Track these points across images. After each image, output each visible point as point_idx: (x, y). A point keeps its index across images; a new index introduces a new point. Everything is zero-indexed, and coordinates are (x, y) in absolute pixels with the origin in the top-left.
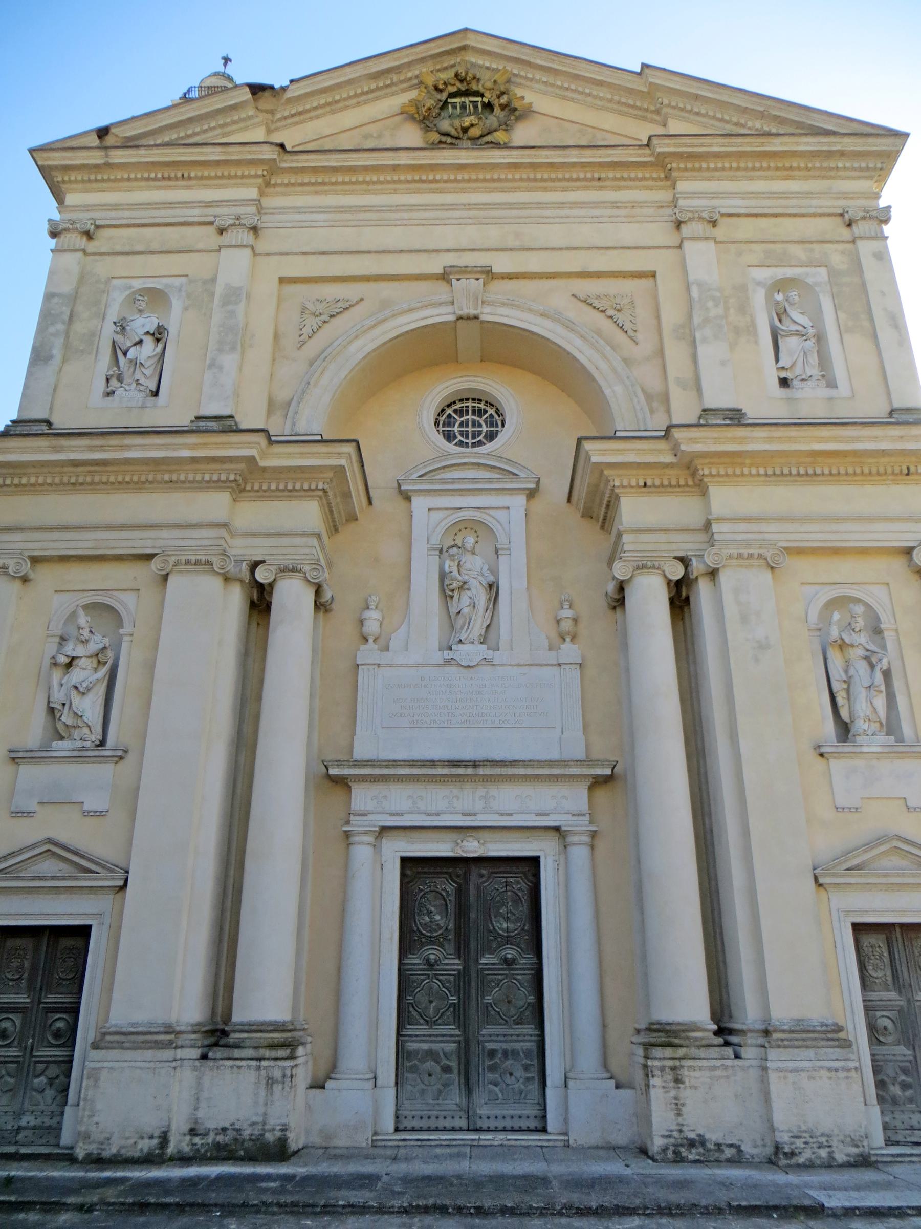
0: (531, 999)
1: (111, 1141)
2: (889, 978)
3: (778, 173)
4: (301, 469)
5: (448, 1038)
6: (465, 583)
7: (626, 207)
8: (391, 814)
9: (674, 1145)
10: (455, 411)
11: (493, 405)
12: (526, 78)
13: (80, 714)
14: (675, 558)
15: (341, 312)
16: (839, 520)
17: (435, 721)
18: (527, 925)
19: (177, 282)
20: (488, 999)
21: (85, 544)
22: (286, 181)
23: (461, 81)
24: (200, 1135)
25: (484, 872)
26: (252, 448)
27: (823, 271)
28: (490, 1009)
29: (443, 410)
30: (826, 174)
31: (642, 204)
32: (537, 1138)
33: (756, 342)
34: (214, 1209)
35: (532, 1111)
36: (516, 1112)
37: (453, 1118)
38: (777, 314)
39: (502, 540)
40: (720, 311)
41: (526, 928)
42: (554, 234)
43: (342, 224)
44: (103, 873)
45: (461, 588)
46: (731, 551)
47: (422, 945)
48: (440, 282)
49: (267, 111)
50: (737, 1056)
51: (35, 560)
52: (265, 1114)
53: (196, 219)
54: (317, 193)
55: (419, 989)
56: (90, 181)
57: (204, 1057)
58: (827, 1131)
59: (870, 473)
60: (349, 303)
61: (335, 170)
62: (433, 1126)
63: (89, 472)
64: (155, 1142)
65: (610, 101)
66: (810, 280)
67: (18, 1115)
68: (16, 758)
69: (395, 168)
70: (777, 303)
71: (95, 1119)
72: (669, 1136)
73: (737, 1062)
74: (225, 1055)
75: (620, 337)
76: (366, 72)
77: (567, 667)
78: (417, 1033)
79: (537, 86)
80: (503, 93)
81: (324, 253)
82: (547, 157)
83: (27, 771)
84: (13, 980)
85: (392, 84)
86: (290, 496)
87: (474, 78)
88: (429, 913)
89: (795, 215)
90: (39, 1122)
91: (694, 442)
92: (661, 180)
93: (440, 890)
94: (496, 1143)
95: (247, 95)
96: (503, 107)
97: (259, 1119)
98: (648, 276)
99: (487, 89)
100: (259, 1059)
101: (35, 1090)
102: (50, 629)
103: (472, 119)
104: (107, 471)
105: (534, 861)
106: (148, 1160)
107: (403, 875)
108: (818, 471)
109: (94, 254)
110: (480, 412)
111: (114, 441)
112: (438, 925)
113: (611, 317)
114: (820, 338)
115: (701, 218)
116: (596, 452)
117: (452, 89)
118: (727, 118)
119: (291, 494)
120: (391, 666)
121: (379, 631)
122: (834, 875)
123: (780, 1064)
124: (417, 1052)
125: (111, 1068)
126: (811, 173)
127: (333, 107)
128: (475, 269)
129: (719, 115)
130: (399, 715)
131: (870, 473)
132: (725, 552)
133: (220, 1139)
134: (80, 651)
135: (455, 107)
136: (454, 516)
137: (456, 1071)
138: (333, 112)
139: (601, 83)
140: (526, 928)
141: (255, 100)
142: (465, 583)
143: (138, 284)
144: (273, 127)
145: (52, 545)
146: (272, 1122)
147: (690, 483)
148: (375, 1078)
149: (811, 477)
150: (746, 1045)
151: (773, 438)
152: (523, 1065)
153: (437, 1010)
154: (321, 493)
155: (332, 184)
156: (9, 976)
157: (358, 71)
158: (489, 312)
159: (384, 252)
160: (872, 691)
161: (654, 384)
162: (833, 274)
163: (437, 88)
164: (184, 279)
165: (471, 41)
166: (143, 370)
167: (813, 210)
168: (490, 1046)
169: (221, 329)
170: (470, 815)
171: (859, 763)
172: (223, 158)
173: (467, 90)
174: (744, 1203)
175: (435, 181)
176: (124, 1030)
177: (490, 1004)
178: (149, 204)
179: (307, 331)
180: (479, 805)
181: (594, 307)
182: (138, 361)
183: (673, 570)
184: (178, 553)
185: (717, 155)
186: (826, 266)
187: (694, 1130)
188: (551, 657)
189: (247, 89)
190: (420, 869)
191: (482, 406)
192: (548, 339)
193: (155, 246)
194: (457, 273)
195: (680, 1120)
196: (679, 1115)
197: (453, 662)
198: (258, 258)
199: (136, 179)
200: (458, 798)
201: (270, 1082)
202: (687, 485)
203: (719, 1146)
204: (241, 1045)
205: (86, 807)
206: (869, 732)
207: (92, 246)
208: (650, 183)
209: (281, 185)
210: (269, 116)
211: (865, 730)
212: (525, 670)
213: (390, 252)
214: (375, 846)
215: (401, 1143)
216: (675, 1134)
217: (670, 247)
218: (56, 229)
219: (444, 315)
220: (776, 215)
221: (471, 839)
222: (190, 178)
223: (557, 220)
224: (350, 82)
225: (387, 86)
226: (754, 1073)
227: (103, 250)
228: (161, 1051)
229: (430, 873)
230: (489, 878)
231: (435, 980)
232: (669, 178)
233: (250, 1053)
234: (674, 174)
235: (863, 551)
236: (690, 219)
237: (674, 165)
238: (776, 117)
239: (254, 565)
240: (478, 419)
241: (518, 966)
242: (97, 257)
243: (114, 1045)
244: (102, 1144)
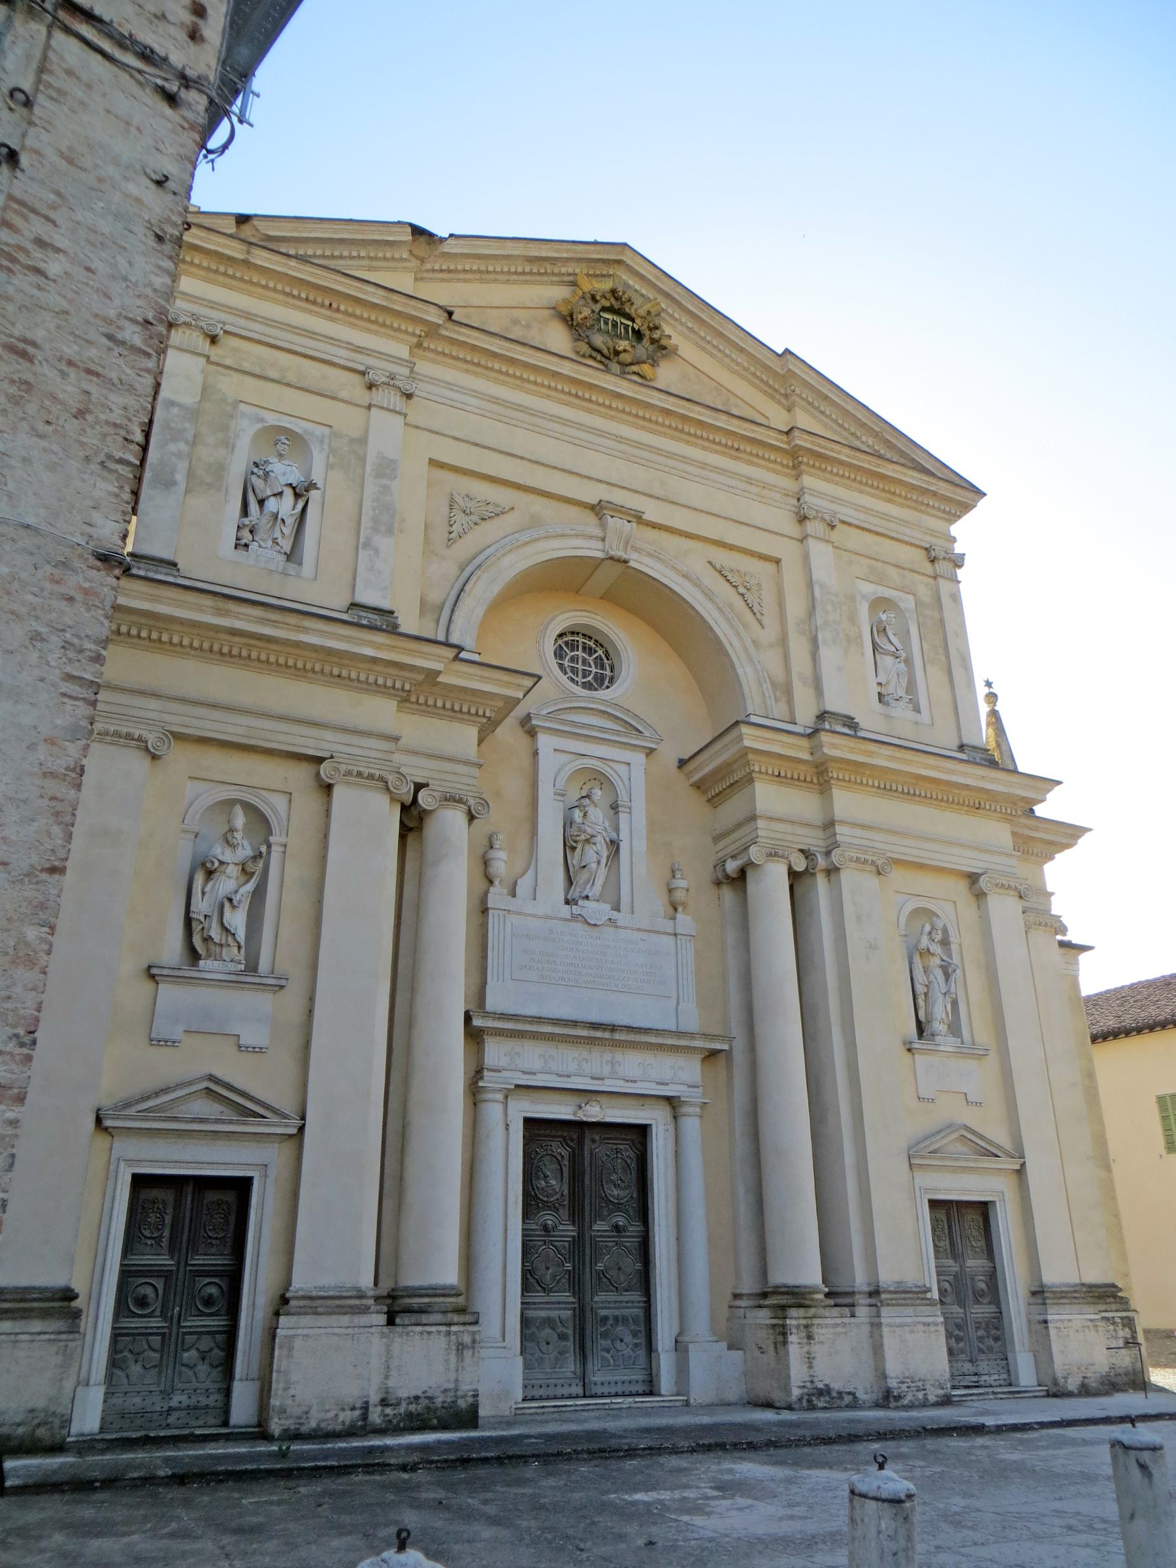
0: (639, 1266)
1: (309, 1415)
2: (948, 1247)
3: (884, 495)
4: (474, 692)
6: (593, 836)
7: (757, 486)
8: (525, 1073)
9: (808, 1395)
10: (566, 643)
12: (672, 316)
13: (233, 932)
14: (802, 851)
16: (928, 839)
19: (319, 430)
20: (600, 1266)
21: (234, 728)
22: (440, 349)
23: (617, 299)
24: (391, 1405)
27: (911, 597)
28: (601, 1275)
30: (918, 506)
34: (531, 1460)
35: (639, 1376)
36: (626, 1377)
37: (570, 1385)
42: (693, 493)
44: (275, 1119)
45: (587, 841)
46: (852, 854)
48: (588, 513)
50: (853, 1316)
52: (457, 1380)
53: (342, 362)
54: (467, 371)
56: (217, 271)
61: (494, 355)
62: (552, 1395)
64: (357, 1413)
65: (746, 369)
66: (901, 605)
67: (166, 1394)
69: (555, 374)
70: (881, 622)
71: (292, 1392)
72: (804, 1387)
73: (852, 1320)
74: (413, 1321)
76: (525, 253)
77: (683, 938)
79: (680, 328)
81: (477, 445)
82: (699, 413)
86: (452, 717)
88: (546, 1177)
89: (892, 538)
90: (193, 1401)
92: (787, 467)
93: (555, 1154)
94: (625, 1406)
97: (451, 1386)
98: (771, 561)
100: (449, 1325)
101: (187, 1366)
102: (186, 822)
105: (643, 1130)
106: (350, 1432)
109: (218, 364)
110: (591, 651)
111: (292, 619)
112: (554, 1190)
113: (742, 595)
114: (908, 662)
115: (823, 519)
118: (846, 425)
119: (455, 714)
120: (519, 914)
122: (922, 1157)
123: (890, 1320)
125: (306, 1335)
126: (908, 503)
129: (840, 422)
133: (412, 1408)
135: (606, 323)
136: (578, 762)
138: (482, 281)
139: (742, 350)
140: (634, 1196)
142: (593, 836)
143: (272, 419)
145: (195, 722)
146: (465, 1387)
147: (815, 781)
149: (910, 795)
150: (858, 1305)
152: (631, 1331)
153: (554, 1276)
155: (487, 368)
159: (537, 463)
161: (778, 673)
162: (918, 603)
164: (327, 430)
165: (628, 258)
168: (603, 1313)
169: (375, 504)
170: (598, 1079)
172: (384, 303)
173: (619, 309)
174: (935, 1427)
176: (314, 1294)
177: (602, 1271)
180: (606, 1070)
182: (279, 517)
184: (350, 762)
185: (841, 463)
189: (409, 230)
191: (591, 643)
192: (687, 602)
193: (291, 377)
194: (611, 510)
195: (811, 1372)
196: (810, 1367)
199: (275, 290)
201: (461, 1348)
202: (811, 782)
203: (840, 1393)
204: (429, 1309)
207: (216, 353)
208: (778, 467)
212: (645, 935)
213: (543, 464)
214: (701, 1117)
215: (539, 1411)
216: (808, 1384)
217: (792, 538)
219: (592, 549)
220: (878, 534)
221: (594, 1104)
222: (338, 310)
224: (507, 257)
225: (539, 274)
226: (866, 1329)
228: (357, 1316)
229: (546, 1136)
232: (796, 470)
233: (438, 1318)
234: (803, 467)
235: (940, 870)
238: (887, 441)
239: (419, 787)
243: (306, 1310)
244: (300, 1418)
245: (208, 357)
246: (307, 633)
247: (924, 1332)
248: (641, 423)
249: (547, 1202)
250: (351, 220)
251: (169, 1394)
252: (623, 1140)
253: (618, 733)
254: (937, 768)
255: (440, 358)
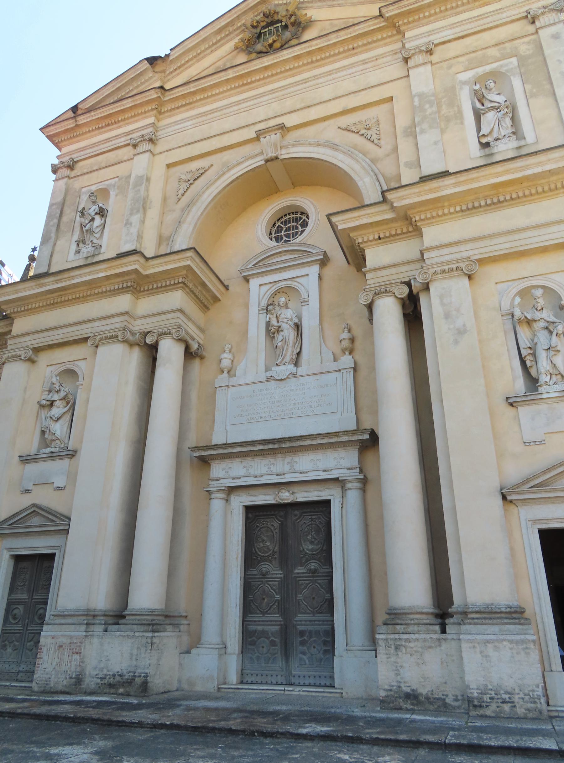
1: (51, 680)
5: (274, 623)
7: (372, 61)
11: (305, 214)
15: (200, 176)
17: (261, 417)
18: (325, 546)
19: (113, 181)
23: (267, 17)
25: (296, 512)
26: (135, 264)
27: (514, 60)
28: (301, 603)
29: (275, 224)
31: (383, 56)
32: (322, 690)
33: (462, 123)
38: (479, 100)
39: (304, 295)
40: (434, 109)
41: (324, 548)
43: (201, 124)
44: (59, 521)
46: (436, 269)
47: (259, 562)
49: (161, 72)
51: (37, 350)
55: (257, 591)
57: (106, 630)
58: (509, 690)
59: (544, 191)
60: (205, 169)
63: (59, 296)
66: (503, 70)
68: (25, 460)
69: (227, 81)
75: (369, 146)
76: (213, 31)
77: (345, 371)
78: (255, 620)
80: (291, 15)
83: (30, 468)
84: (20, 586)
85: (230, 33)
87: (275, 13)
91: (403, 199)
93: (269, 526)
95: (146, 65)
96: (293, 24)
99: (283, 17)
101: (28, 650)
103: (274, 37)
104: (67, 294)
105: (327, 503)
107: (247, 518)
108: (502, 199)
109: (74, 177)
112: (268, 549)
113: (363, 135)
114: (514, 109)
115: (421, 51)
116: (340, 222)
117: (263, 24)
119: (166, 288)
121: (230, 366)
122: (518, 493)
124: (255, 631)
127: (197, 58)
128: (274, 128)
130: (240, 416)
131: (544, 191)
132: (432, 271)
134: (56, 397)
137: (279, 645)
138: (198, 61)
141: (153, 67)
144: (165, 80)
147: (411, 229)
148: (226, 648)
151: (459, 182)
154: (181, 285)
156: (19, 584)
157: (209, 31)
158: (285, 152)
159: (223, 133)
160: (550, 351)
162: (522, 60)
163: (253, 26)
164: (117, 179)
166: (94, 234)
167: (504, 21)
168: (300, 628)
171: (543, 407)
175: (252, 82)
177: (301, 600)
178: (99, 142)
179: (181, 191)
181: (352, 131)
183: (401, 291)
186: (516, 56)
187: (409, 686)
188: (334, 366)
189: (146, 62)
190: (257, 514)
192: (322, 160)
195: (399, 678)
197: (272, 378)
198: (156, 157)
200: (274, 464)
205: (55, 485)
206: (551, 383)
209: (167, 111)
210: (163, 74)
211: (546, 382)
212: (318, 377)
214: (227, 501)
217: (401, 78)
218: (54, 168)
219: (259, 161)
221: (283, 491)
223: (328, 83)
225: (227, 35)
227: (78, 174)
230: (301, 516)
231: (267, 585)
235: (544, 250)
236: (413, 54)
237: (400, 23)
240: (296, 224)
241: (319, 574)
242: (76, 179)
245: (68, 177)
246: (75, 279)
247: (511, 649)
248: (286, 74)
249: (264, 557)
250: (117, 77)
251: (19, 664)
252: (314, 512)
253: (294, 259)
254: (507, 172)
255: (173, 112)
